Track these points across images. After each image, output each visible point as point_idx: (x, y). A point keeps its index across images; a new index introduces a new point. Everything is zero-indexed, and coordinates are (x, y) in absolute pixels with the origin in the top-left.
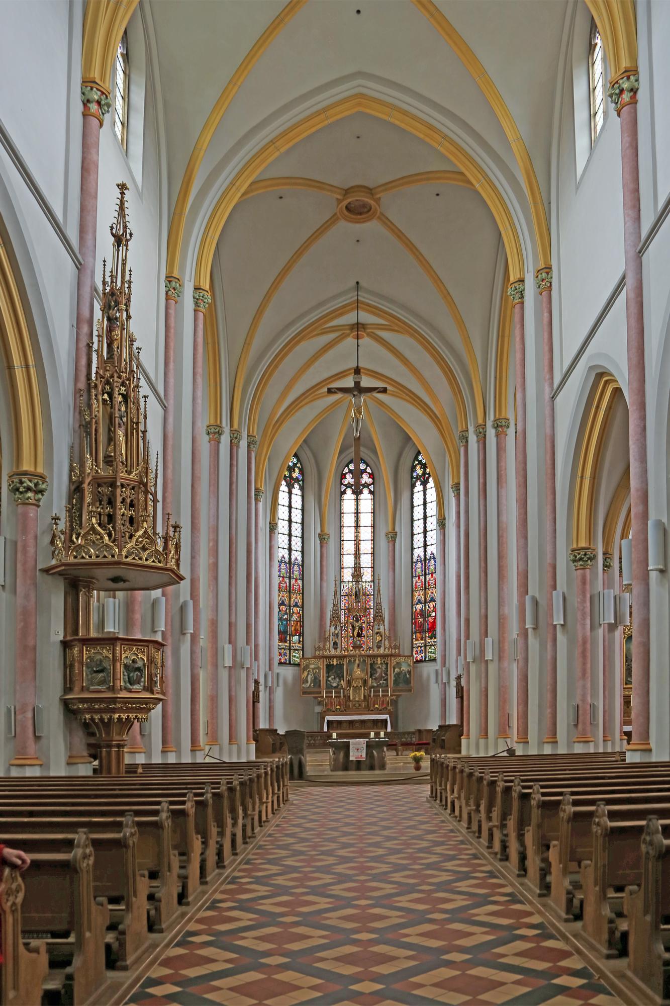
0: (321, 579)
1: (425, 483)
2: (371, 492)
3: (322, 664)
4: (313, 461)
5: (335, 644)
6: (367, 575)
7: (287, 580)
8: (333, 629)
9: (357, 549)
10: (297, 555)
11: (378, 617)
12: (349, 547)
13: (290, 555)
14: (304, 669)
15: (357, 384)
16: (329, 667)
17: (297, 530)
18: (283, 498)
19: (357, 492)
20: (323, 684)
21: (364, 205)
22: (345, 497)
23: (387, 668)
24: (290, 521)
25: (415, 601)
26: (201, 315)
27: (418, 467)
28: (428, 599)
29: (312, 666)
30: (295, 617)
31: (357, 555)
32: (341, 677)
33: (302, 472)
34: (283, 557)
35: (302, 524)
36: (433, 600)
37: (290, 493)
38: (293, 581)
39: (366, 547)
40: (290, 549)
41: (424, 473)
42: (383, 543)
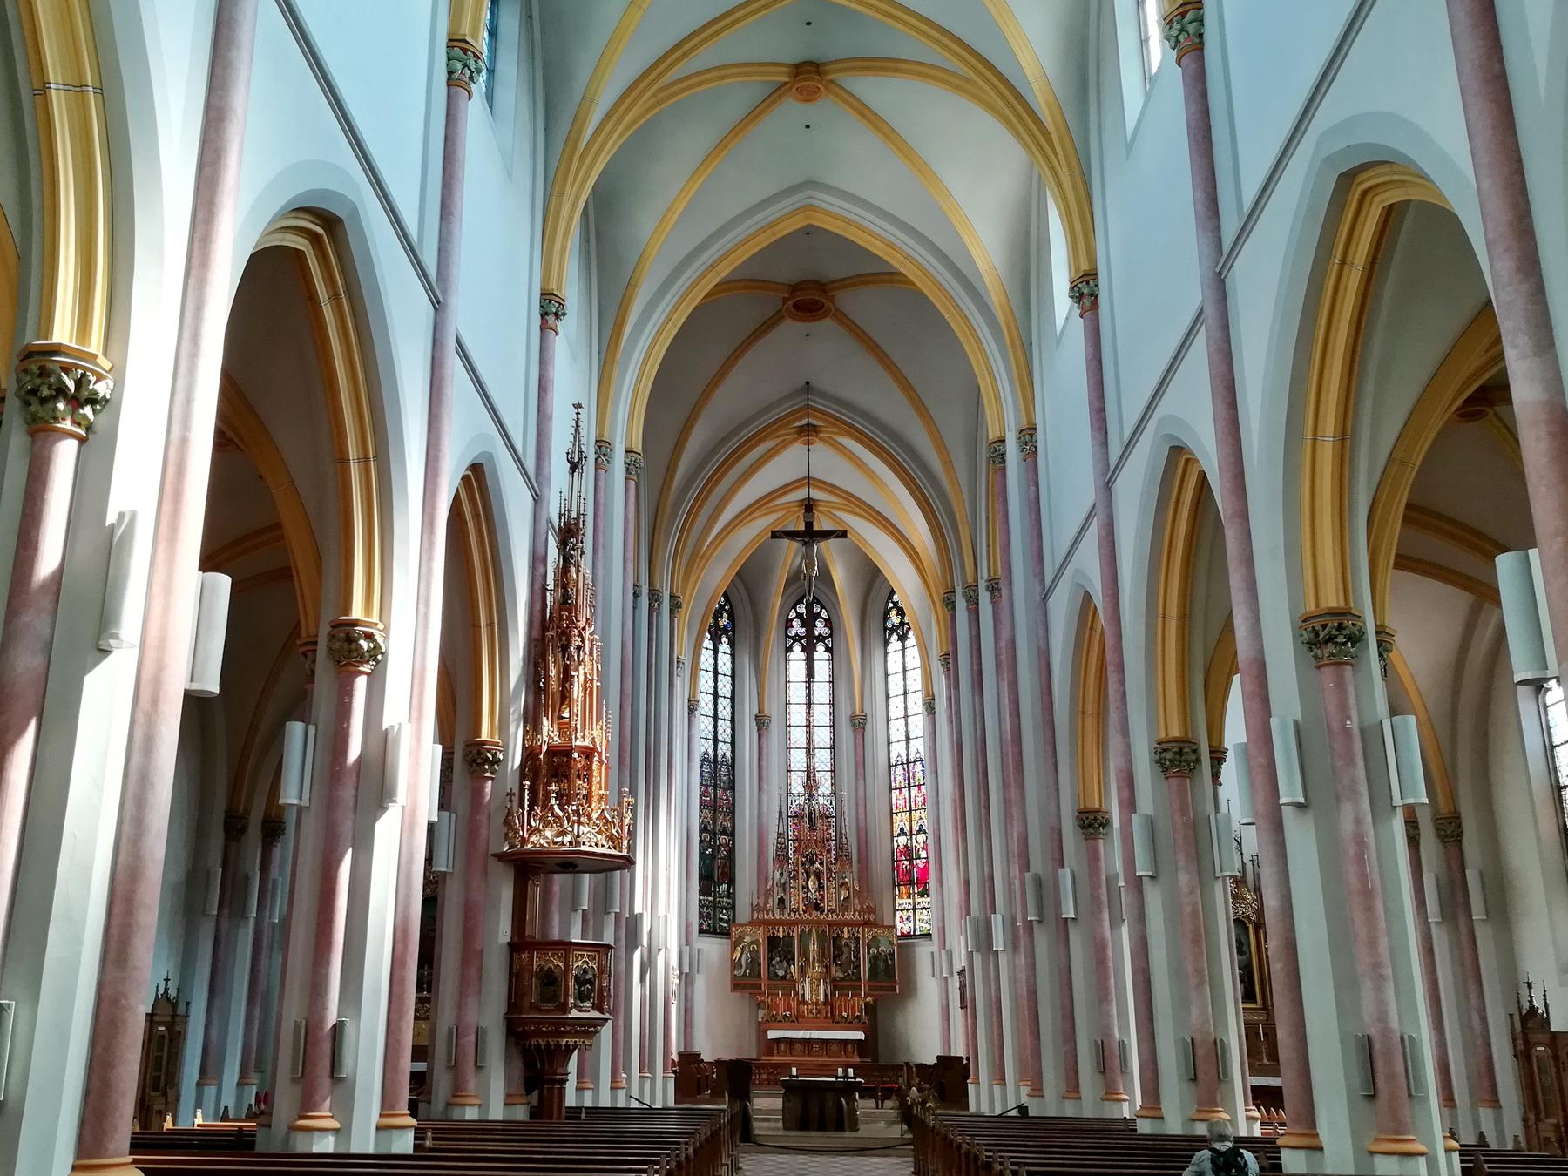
0: (760, 790)
1: (902, 638)
2: (828, 650)
3: (761, 934)
4: (745, 596)
5: (781, 901)
6: (825, 786)
7: (711, 790)
9: (810, 740)
10: (724, 749)
11: (843, 855)
12: (798, 736)
13: (715, 749)
14: (736, 944)
15: (809, 525)
16: (773, 940)
18: (706, 658)
20: (764, 972)
21: (816, 302)
22: (792, 656)
23: (857, 947)
24: (716, 695)
25: (897, 830)
26: (632, 484)
27: (894, 612)
28: (916, 828)
29: (747, 939)
33: (734, 620)
34: (706, 753)
35: (733, 699)
36: (921, 830)
37: (716, 651)
38: (719, 792)
39: (823, 736)
40: (715, 740)
41: (902, 624)
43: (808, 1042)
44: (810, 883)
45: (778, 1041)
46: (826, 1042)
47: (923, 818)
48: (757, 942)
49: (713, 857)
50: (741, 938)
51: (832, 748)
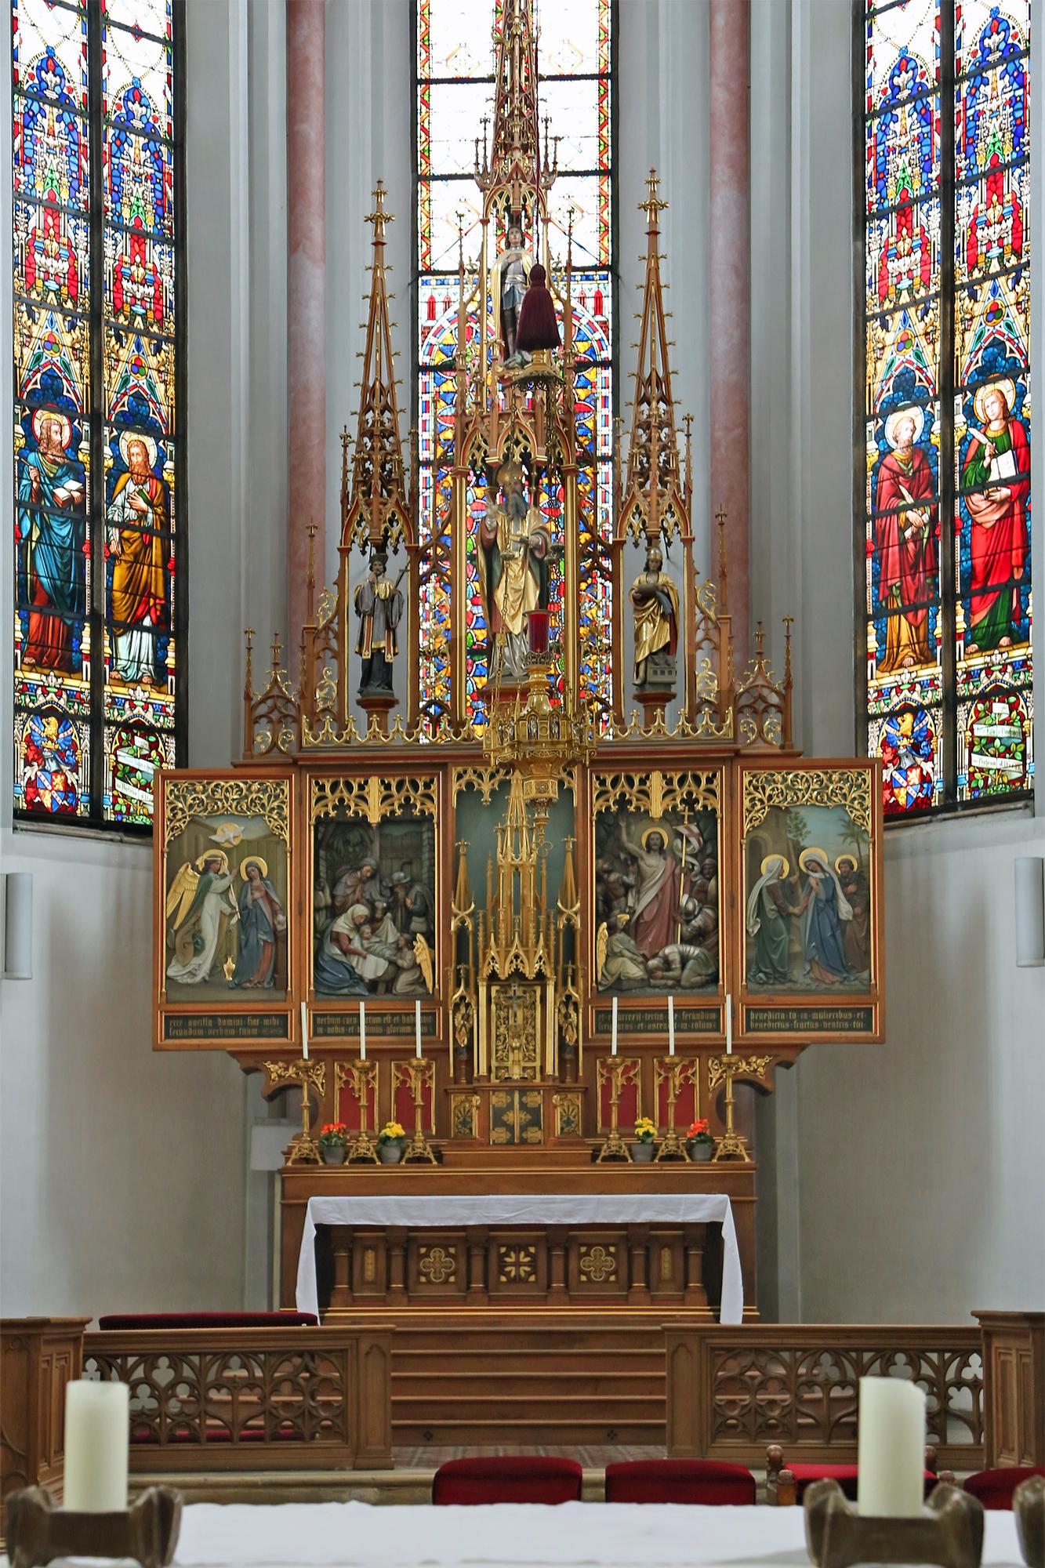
0: (295, 242)
3: (287, 812)
5: (377, 671)
8: (359, 563)
13: (94, 54)
16: (338, 837)
29: (229, 832)
30: (129, 501)
34: (49, 62)
36: (999, 363)
38: (115, 247)
43: (477, 1244)
48: (269, 844)
49: (88, 514)
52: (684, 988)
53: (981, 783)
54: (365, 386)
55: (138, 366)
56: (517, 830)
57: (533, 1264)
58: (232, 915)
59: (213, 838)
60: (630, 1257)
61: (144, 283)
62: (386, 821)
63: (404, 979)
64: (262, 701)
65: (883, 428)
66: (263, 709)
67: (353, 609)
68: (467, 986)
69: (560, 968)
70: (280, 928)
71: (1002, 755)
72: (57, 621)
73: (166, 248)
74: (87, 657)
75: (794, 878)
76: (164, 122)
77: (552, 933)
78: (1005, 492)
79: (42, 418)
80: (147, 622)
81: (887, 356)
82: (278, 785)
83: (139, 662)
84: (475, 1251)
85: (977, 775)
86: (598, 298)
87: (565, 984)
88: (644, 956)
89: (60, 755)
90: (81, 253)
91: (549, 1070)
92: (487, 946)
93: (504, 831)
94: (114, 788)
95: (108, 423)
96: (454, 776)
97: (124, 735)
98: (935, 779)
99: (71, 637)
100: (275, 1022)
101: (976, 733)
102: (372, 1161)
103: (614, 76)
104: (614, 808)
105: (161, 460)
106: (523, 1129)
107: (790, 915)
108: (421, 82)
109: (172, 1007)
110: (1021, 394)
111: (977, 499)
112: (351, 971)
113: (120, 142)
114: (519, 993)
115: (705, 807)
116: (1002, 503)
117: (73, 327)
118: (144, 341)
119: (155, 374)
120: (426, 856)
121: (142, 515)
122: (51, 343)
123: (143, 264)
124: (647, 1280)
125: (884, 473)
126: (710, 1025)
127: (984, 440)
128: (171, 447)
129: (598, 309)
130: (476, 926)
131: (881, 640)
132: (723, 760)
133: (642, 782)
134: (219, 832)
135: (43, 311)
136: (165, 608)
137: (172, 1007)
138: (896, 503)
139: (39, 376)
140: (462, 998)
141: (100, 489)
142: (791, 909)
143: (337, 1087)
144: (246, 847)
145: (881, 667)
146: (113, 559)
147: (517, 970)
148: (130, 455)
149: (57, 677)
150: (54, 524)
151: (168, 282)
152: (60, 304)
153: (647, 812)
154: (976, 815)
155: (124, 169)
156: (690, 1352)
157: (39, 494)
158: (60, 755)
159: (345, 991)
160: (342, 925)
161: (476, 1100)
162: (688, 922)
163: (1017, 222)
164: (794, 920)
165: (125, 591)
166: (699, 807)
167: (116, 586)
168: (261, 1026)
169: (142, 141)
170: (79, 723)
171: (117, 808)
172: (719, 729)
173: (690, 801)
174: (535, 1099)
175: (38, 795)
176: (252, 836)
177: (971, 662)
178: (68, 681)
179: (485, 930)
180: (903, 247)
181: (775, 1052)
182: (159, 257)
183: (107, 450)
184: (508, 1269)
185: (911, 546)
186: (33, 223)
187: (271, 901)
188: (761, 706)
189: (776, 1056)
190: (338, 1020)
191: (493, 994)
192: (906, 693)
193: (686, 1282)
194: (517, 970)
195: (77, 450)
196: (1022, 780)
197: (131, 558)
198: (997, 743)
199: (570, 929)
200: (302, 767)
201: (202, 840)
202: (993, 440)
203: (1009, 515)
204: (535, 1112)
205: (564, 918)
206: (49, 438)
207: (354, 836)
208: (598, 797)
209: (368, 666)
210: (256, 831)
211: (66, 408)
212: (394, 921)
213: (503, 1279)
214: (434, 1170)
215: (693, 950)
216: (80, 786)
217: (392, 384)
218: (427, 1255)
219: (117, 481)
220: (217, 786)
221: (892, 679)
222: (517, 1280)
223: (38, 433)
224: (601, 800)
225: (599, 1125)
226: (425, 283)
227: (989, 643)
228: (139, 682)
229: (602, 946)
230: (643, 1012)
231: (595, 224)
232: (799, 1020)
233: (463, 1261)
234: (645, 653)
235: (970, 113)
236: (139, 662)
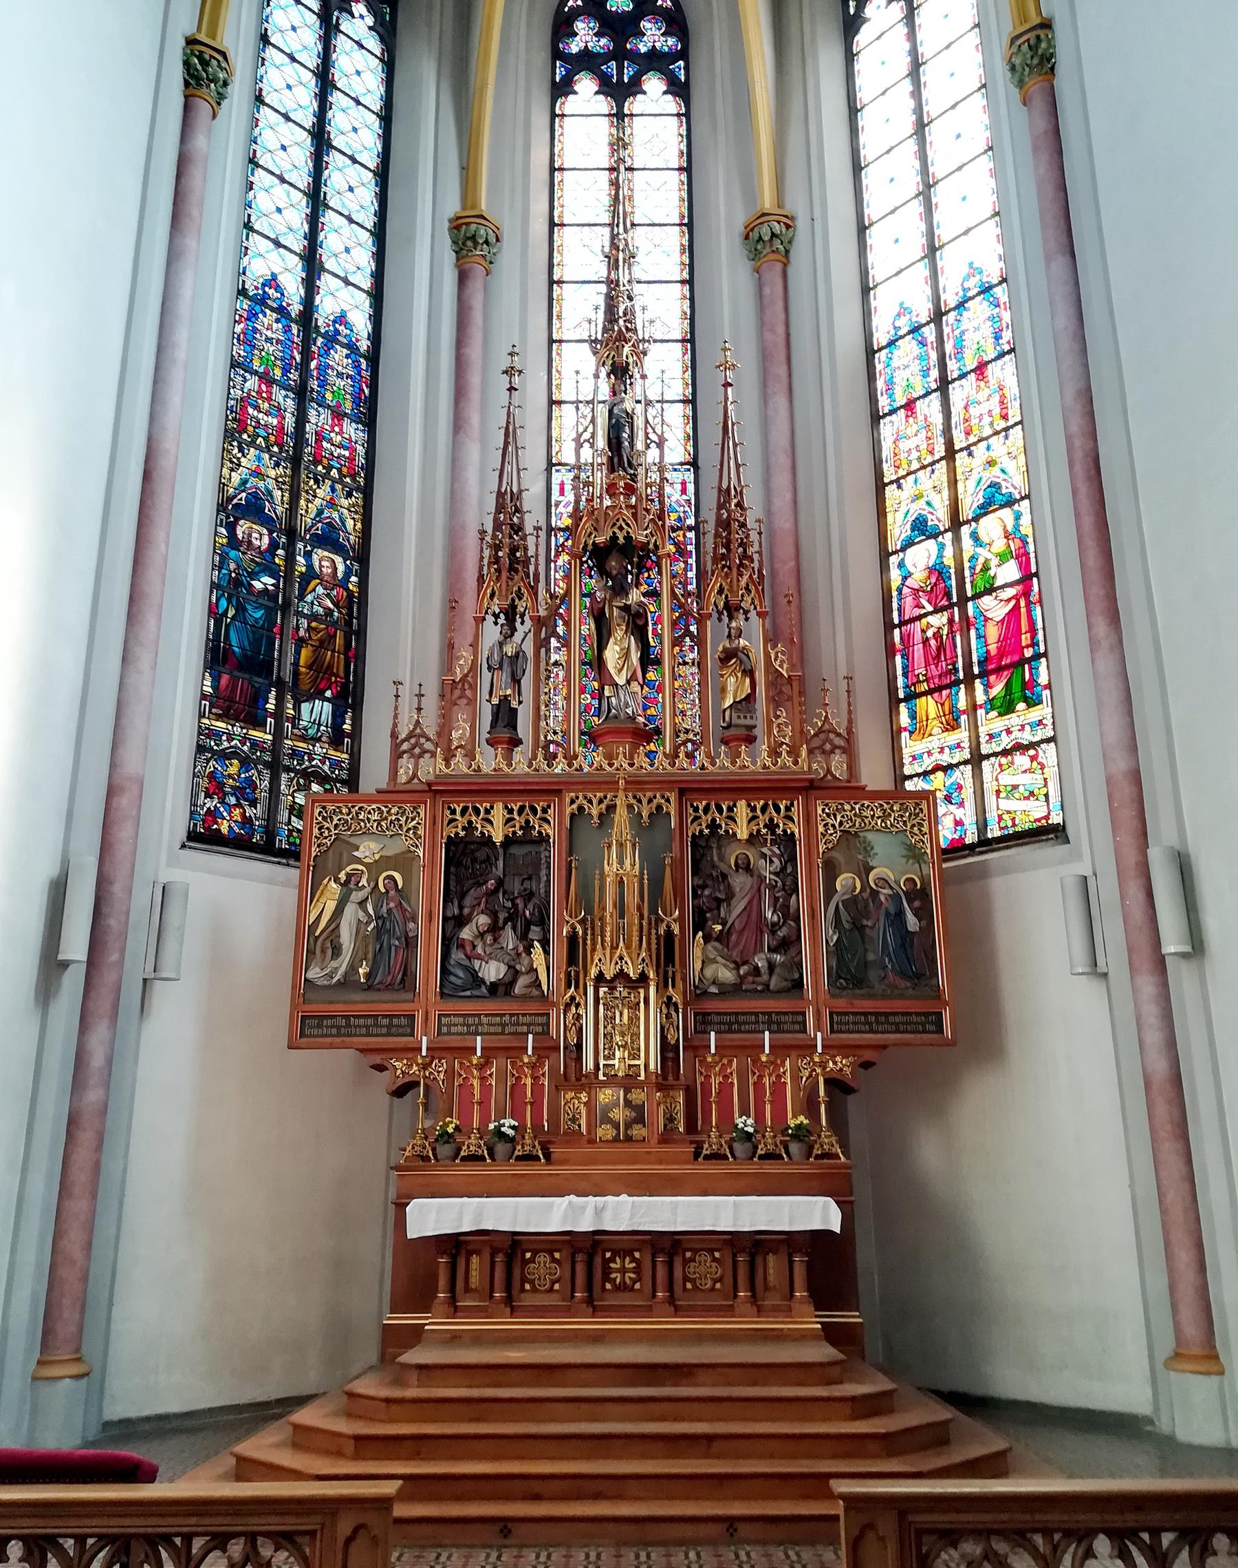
2: (679, 89)
5: (505, 715)
8: (492, 632)
10: (345, 303)
16: (465, 858)
17: (351, 189)
19: (620, 92)
22: (570, 104)
29: (368, 849)
30: (318, 599)
31: (619, 216)
32: (530, 922)
36: (995, 500)
38: (317, 418)
42: (730, 273)
43: (588, 1249)
44: (612, 654)
45: (453, 1246)
46: (669, 1246)
47: (1004, 459)
48: (404, 861)
49: (279, 604)
50: (342, 848)
51: (690, 340)
52: (772, 992)
53: (1010, 824)
54: (499, 491)
55: (332, 504)
56: (621, 845)
57: (637, 1270)
58: (368, 923)
59: (355, 853)
60: (735, 1263)
61: (340, 446)
62: (508, 841)
63: (522, 981)
64: (407, 739)
65: (903, 559)
66: (405, 746)
67: (485, 666)
68: (577, 987)
69: (661, 971)
70: (411, 934)
71: (1027, 798)
72: (246, 682)
73: (360, 426)
74: (272, 715)
75: (865, 895)
76: (364, 345)
77: (653, 937)
78: (1011, 592)
79: (242, 529)
80: (328, 694)
81: (904, 509)
82: (415, 808)
83: (319, 725)
84: (579, 1257)
85: (1005, 817)
86: (684, 484)
87: (666, 986)
88: (735, 962)
89: (239, 791)
90: (288, 415)
91: (652, 1066)
92: (594, 950)
93: (610, 846)
94: (289, 823)
95: (303, 539)
96: (568, 800)
97: (302, 781)
98: (966, 822)
99: (258, 698)
100: (403, 1021)
101: (1002, 782)
102: (482, 1158)
103: (692, 341)
104: (706, 831)
105: (348, 573)
106: (628, 1126)
107: (863, 927)
108: (556, 341)
109: (307, 1008)
110: (1018, 517)
111: (987, 601)
112: (474, 974)
113: (328, 349)
114: (625, 994)
115: (785, 831)
116: (1009, 600)
117: (277, 465)
118: (338, 487)
119: (345, 512)
120: (543, 873)
121: (329, 612)
122: (257, 473)
123: (341, 433)
124: (752, 1288)
125: (905, 590)
126: (797, 1027)
127: (989, 556)
128: (356, 566)
129: (684, 491)
130: (585, 933)
131: (913, 716)
132: (799, 790)
133: (730, 809)
134: (361, 849)
135: (252, 450)
136: (345, 686)
137: (307, 1008)
138: (917, 612)
139: (244, 495)
140: (573, 998)
141: (292, 586)
142: (865, 922)
143: (456, 1084)
144: (384, 863)
145: (914, 736)
146: (300, 643)
147: (622, 970)
148: (321, 566)
149: (242, 728)
150: (249, 607)
151: (361, 450)
152: (267, 447)
153: (735, 834)
154: (381, 1283)
155: (329, 366)
156: (882, 1539)
157: (237, 583)
158: (239, 791)
159: (468, 993)
160: (466, 934)
161: (584, 1097)
162: (773, 933)
163: (1003, 397)
164: (868, 931)
165: (310, 667)
166: (779, 831)
167: (302, 662)
168: (390, 1026)
169: (345, 351)
170: (260, 767)
171: (292, 840)
172: (796, 763)
173: (772, 826)
174: (638, 1096)
175: (217, 823)
176: (389, 853)
177: (991, 726)
178: (251, 732)
179: (593, 934)
180: (911, 431)
181: (859, 1052)
182: (353, 430)
183: (301, 559)
184: (613, 1276)
185: (933, 642)
186: (248, 385)
187: (404, 911)
188: (828, 747)
189: (859, 1056)
190: (461, 1019)
191: (601, 994)
192: (936, 756)
193: (792, 1290)
194: (622, 970)
195: (274, 555)
196: (1047, 818)
197: (317, 644)
198: (1021, 789)
199: (669, 932)
200: (437, 792)
201: (345, 855)
202: (997, 555)
203: (1017, 608)
204: (639, 1109)
205: (664, 925)
206: (250, 542)
207: (481, 854)
208: (692, 822)
209: (497, 712)
210: (395, 847)
211: (267, 522)
212: (514, 928)
213: (608, 1286)
214: (540, 1169)
215: (778, 958)
216: (257, 819)
217: (520, 491)
218: (532, 1260)
219: (309, 584)
220: (360, 809)
221: (924, 745)
222: (623, 1288)
223: (240, 537)
224: (695, 824)
225: (700, 1122)
226: (557, 471)
227: (1007, 708)
228: (319, 740)
229: (698, 953)
230: (737, 1014)
231: (681, 435)
232: (878, 1023)
233: (568, 1267)
234: (728, 702)
235: (957, 332)
236: (319, 725)
